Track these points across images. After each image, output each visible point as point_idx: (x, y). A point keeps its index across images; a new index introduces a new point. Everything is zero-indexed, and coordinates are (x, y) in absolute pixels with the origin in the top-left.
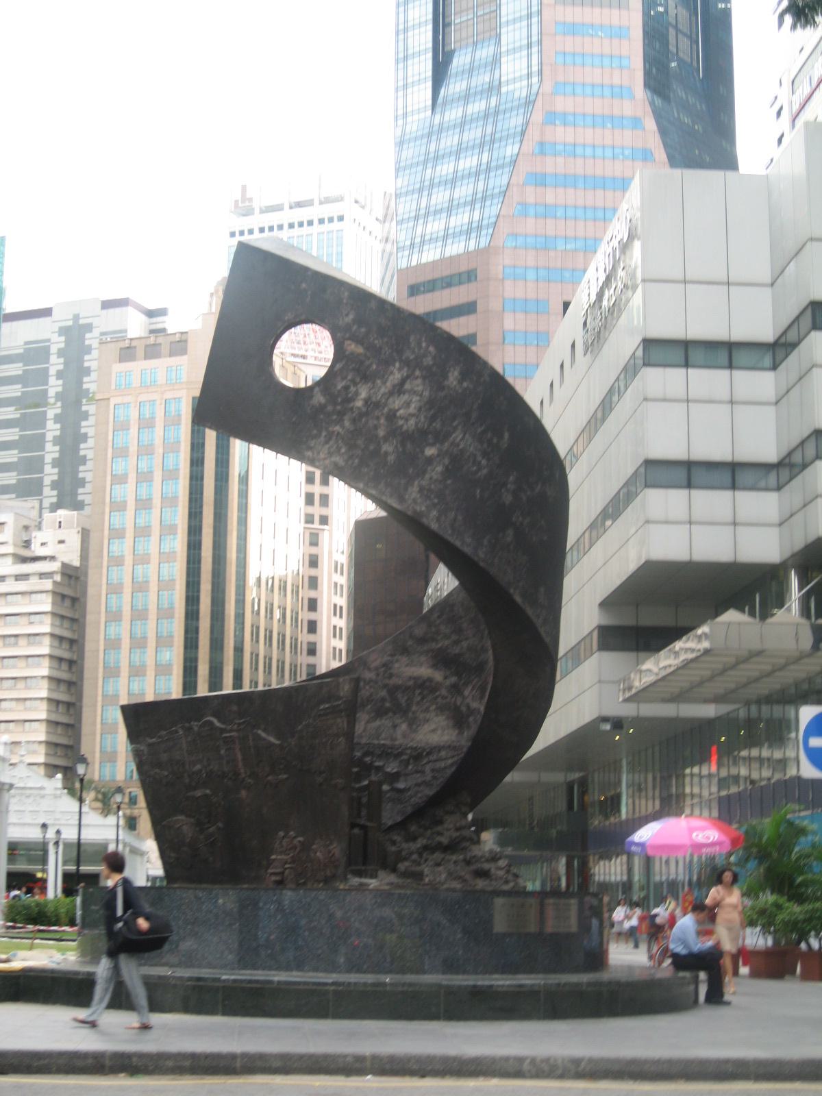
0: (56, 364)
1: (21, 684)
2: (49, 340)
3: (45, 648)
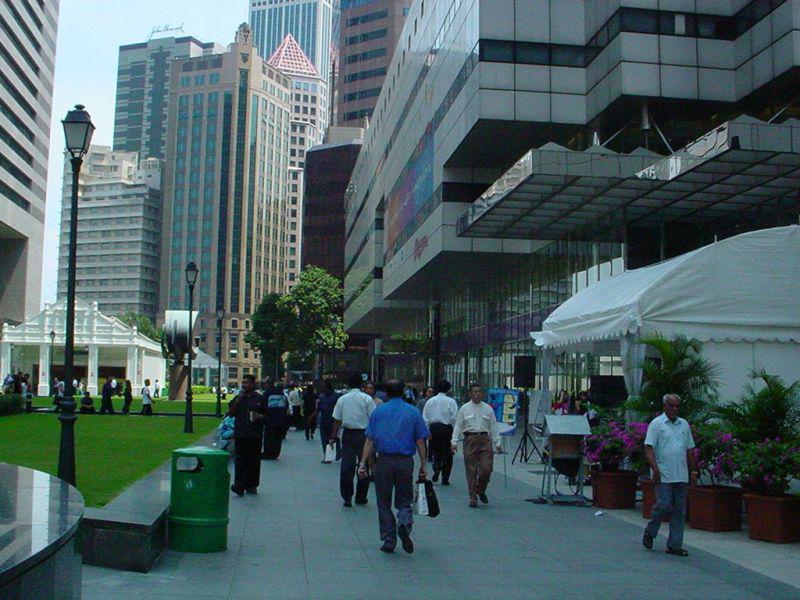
0: (149, 75)
1: (124, 283)
2: (145, 61)
3: (137, 287)
